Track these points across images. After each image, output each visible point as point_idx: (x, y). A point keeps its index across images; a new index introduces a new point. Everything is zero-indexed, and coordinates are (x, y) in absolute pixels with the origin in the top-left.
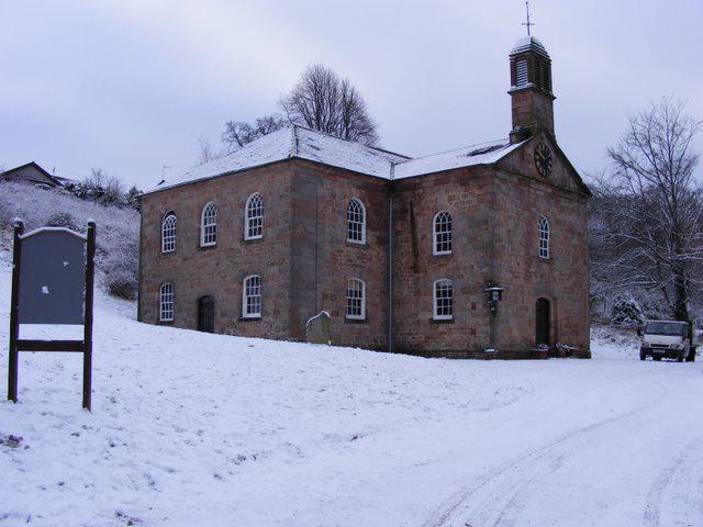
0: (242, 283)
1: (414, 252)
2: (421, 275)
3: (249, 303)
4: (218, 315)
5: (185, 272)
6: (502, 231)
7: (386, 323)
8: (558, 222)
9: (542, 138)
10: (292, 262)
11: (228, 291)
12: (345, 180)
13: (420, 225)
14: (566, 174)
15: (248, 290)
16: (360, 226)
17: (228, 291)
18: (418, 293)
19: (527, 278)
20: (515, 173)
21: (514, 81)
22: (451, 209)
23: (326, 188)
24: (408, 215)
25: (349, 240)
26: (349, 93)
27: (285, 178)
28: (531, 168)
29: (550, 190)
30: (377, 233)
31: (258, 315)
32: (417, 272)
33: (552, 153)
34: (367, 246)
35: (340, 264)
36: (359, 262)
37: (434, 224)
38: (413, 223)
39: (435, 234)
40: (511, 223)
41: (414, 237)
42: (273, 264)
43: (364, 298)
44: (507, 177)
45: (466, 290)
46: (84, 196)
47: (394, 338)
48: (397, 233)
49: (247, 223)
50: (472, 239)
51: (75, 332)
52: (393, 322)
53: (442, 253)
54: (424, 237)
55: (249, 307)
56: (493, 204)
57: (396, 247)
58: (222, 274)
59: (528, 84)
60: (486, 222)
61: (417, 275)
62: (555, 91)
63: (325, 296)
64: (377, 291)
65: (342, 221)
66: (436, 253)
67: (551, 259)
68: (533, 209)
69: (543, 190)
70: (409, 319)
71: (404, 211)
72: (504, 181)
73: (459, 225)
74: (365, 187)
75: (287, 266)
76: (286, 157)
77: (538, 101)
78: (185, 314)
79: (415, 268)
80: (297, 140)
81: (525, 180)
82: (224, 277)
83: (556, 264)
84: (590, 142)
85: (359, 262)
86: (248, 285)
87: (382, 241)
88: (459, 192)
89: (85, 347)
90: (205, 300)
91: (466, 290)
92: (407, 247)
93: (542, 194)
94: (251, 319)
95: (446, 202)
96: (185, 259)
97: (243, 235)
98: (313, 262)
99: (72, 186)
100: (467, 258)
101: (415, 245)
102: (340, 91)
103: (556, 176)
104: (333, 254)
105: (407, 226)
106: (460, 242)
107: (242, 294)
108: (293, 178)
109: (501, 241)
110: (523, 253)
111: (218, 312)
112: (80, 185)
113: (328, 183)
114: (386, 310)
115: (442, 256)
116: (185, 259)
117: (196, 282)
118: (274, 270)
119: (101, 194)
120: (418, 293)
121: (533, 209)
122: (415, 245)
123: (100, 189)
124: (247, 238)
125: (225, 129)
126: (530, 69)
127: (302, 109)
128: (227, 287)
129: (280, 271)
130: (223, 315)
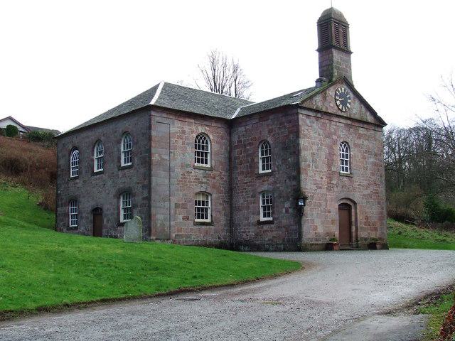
19: (330, 189)
34: (211, 169)
40: (315, 147)
63: (177, 206)
65: (191, 152)
66: (261, 171)
68: (334, 137)
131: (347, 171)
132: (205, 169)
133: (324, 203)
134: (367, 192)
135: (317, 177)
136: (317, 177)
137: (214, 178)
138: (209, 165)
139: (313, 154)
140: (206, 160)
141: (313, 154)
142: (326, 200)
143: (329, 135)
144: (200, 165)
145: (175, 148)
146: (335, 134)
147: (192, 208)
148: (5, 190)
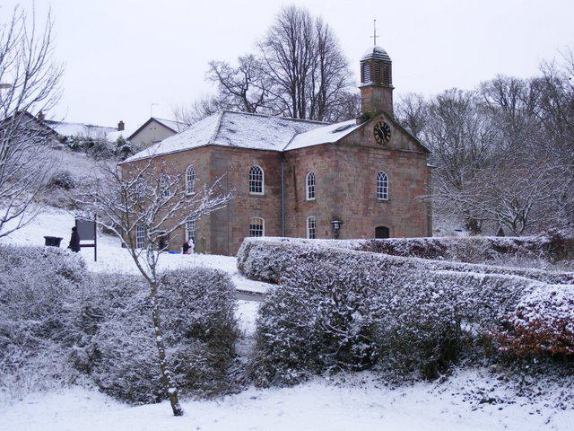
2: (300, 214)
6: (344, 185)
8: (395, 174)
9: (382, 118)
12: (248, 155)
13: (298, 181)
14: (405, 140)
16: (260, 183)
18: (298, 226)
19: (366, 212)
20: (355, 145)
21: (363, 81)
22: (314, 170)
23: (233, 162)
24: (292, 173)
25: (252, 193)
26: (323, 30)
27: (205, 157)
28: (371, 140)
29: (389, 153)
30: (273, 187)
32: (297, 212)
33: (392, 128)
34: (265, 196)
37: (307, 180)
38: (295, 179)
39: (307, 187)
40: (352, 179)
41: (295, 189)
43: (308, 229)
44: (348, 149)
45: (323, 223)
46: (76, 148)
48: (287, 186)
50: (326, 190)
51: (92, 242)
53: (312, 199)
54: (301, 188)
56: (337, 167)
57: (286, 195)
59: (370, 83)
60: (332, 180)
62: (394, 84)
63: (234, 230)
64: (274, 225)
65: (246, 181)
66: (308, 199)
67: (390, 200)
68: (372, 168)
69: (381, 154)
71: (290, 171)
72: (345, 152)
73: (319, 181)
74: (263, 157)
76: (206, 143)
77: (378, 93)
79: (296, 209)
80: (221, 126)
81: (363, 149)
83: (394, 203)
87: (277, 192)
88: (319, 160)
89: (94, 246)
91: (323, 223)
92: (292, 196)
93: (381, 156)
95: (313, 166)
99: (66, 138)
100: (324, 203)
101: (296, 195)
102: (314, 25)
103: (395, 142)
105: (292, 181)
106: (319, 192)
108: (212, 157)
109: (342, 191)
110: (362, 197)
112: (72, 137)
113: (235, 158)
115: (311, 201)
119: (92, 144)
120: (298, 226)
121: (372, 168)
122: (296, 195)
123: (91, 140)
125: (209, 67)
126: (371, 70)
127: (279, 48)
131: (385, 197)
132: (260, 196)
133: (360, 227)
134: (405, 216)
135: (353, 204)
136: (353, 204)
137: (267, 205)
138: (263, 193)
139: (349, 185)
140: (261, 189)
141: (349, 185)
142: (362, 224)
143: (367, 167)
144: (255, 193)
145: (232, 180)
146: (373, 165)
147: (364, 386)
148: (468, 212)
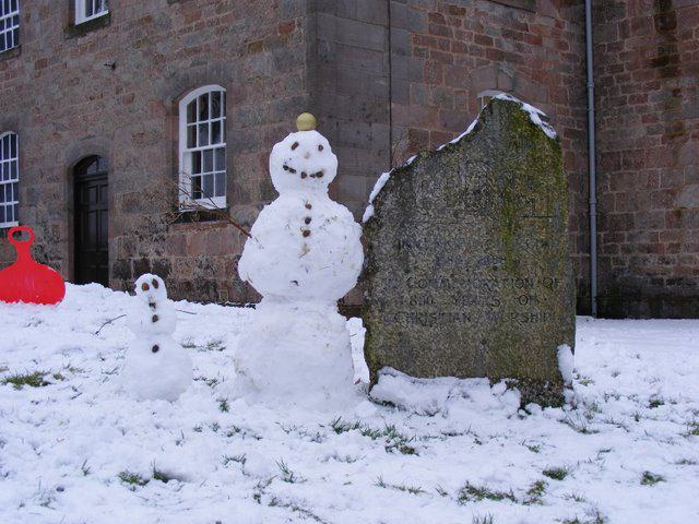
0: (176, 112)
1: (660, 18)
3: (197, 168)
4: (118, 205)
5: (41, 99)
7: (582, 222)
10: (314, 28)
11: (139, 138)
15: (192, 131)
17: (139, 138)
31: (220, 202)
32: (672, 73)
35: (460, 48)
36: (508, 46)
42: (257, 47)
47: (603, 261)
49: (185, 165)
52: (601, 218)
55: (197, 181)
58: (125, 93)
61: (672, 84)
70: (653, 210)
75: (298, 45)
78: (42, 207)
82: (131, 100)
84: (514, 398)
85: (508, 46)
86: (192, 118)
90: (91, 170)
94: (205, 216)
96: (41, 64)
97: (174, 193)
98: (378, 37)
104: (435, 17)
107: (176, 143)
111: (117, 197)
114: (580, 183)
116: (41, 64)
117: (65, 121)
118: (262, 62)
124: (185, 199)
128: (137, 129)
129: (279, 64)
130: (130, 206)
